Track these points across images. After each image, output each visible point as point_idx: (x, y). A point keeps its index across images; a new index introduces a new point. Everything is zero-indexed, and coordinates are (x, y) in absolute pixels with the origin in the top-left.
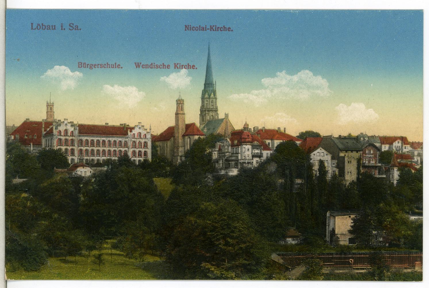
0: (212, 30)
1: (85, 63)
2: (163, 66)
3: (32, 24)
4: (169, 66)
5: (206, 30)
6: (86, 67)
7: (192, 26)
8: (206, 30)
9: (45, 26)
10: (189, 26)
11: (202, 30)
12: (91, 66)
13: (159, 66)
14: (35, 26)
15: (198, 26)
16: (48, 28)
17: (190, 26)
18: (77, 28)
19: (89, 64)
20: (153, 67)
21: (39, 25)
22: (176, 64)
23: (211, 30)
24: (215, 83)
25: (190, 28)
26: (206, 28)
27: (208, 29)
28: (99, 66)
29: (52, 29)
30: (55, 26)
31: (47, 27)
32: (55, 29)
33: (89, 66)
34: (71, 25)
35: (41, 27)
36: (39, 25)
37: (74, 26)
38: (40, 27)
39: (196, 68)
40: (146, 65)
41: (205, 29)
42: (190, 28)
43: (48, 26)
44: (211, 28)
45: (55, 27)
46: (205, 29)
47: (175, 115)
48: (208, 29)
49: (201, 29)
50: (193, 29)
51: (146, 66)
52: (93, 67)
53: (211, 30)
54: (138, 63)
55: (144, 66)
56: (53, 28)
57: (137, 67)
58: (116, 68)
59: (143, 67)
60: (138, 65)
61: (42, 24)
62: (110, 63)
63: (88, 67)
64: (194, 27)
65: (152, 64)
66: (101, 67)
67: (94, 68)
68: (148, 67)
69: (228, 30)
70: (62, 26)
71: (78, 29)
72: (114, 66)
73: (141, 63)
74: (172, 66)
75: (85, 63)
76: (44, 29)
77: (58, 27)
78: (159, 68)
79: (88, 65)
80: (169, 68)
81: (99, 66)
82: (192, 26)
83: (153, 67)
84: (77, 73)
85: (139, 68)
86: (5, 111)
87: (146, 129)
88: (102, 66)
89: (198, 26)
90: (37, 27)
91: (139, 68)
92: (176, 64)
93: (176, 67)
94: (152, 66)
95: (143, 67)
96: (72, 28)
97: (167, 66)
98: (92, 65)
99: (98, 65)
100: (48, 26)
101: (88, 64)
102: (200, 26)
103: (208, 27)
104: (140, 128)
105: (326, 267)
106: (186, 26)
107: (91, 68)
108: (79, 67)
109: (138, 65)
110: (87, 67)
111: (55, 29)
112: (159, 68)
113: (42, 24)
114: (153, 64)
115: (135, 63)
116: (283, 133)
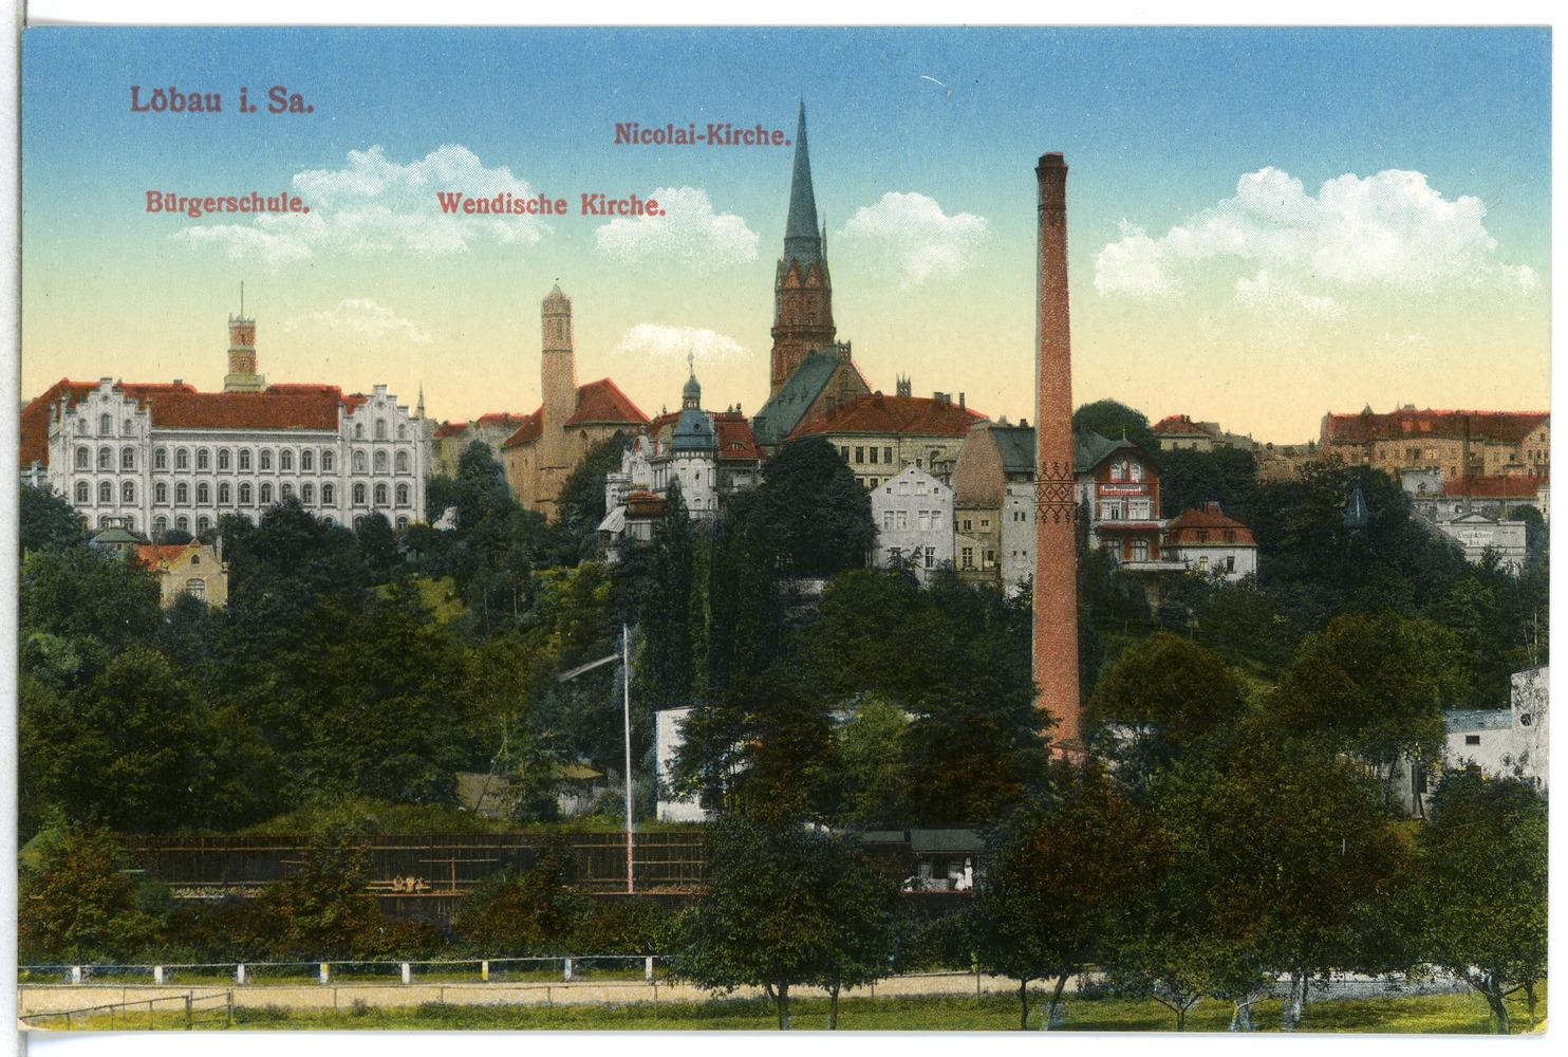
0: (715, 140)
1: (173, 195)
2: (254, 204)
3: (135, 90)
4: (564, 203)
5: (692, 141)
6: (174, 209)
7: (640, 130)
8: (692, 141)
9: (182, 98)
10: (633, 128)
11: (677, 141)
12: (195, 204)
13: (525, 206)
14: (145, 98)
15: (664, 127)
16: (296, 107)
17: (636, 125)
18: (298, 105)
19: (186, 199)
20: (505, 207)
21: (159, 93)
22: (589, 198)
23: (710, 142)
24: (824, 235)
25: (636, 133)
26: (692, 133)
27: (701, 137)
28: (224, 205)
29: (210, 109)
30: (217, 97)
31: (188, 103)
32: (218, 108)
33: (186, 206)
34: (278, 93)
35: (167, 100)
36: (159, 93)
37: (287, 98)
38: (165, 101)
39: (663, 213)
40: (479, 202)
41: (688, 138)
42: (636, 133)
43: (195, 99)
44: (712, 134)
45: (150, 202)
46: (688, 138)
47: (773, 294)
48: (701, 137)
49: (674, 136)
50: (647, 137)
51: (480, 206)
52: (201, 208)
53: (710, 142)
54: (450, 195)
55: (473, 204)
56: (213, 103)
57: (446, 210)
58: (285, 210)
59: (211, 207)
60: (450, 200)
61: (172, 90)
62: (264, 194)
63: (182, 209)
64: (649, 132)
65: (501, 196)
66: (519, 209)
67: (204, 212)
68: (767, 140)
69: (774, 141)
70: (244, 99)
71: (301, 109)
72: (277, 204)
73: (459, 195)
74: (575, 205)
75: (173, 195)
76: (181, 109)
77: (231, 100)
78: (239, 211)
79: (183, 200)
80: (564, 212)
81: (224, 205)
82: (640, 130)
83: (505, 207)
84: (967, 220)
85: (454, 211)
86: (19, 351)
87: (406, 408)
88: (233, 205)
89: (664, 127)
90: (154, 100)
91: (454, 211)
92: (589, 198)
93: (589, 208)
94: (502, 204)
95: (211, 207)
96: (277, 105)
97: (557, 205)
98: (199, 201)
99: (221, 200)
100: (195, 99)
101: (612, 198)
102: (670, 127)
103: (701, 129)
104: (105, 398)
105: (213, 886)
106: (619, 127)
107: (194, 212)
108: (149, 209)
109: (450, 200)
110: (178, 207)
111: (218, 108)
112: (239, 211)
113: (172, 90)
114: (506, 199)
115: (441, 196)
116: (46, 436)
